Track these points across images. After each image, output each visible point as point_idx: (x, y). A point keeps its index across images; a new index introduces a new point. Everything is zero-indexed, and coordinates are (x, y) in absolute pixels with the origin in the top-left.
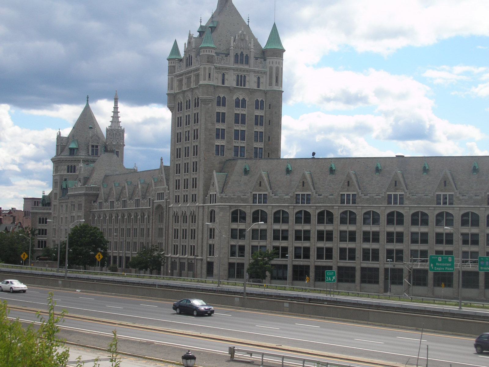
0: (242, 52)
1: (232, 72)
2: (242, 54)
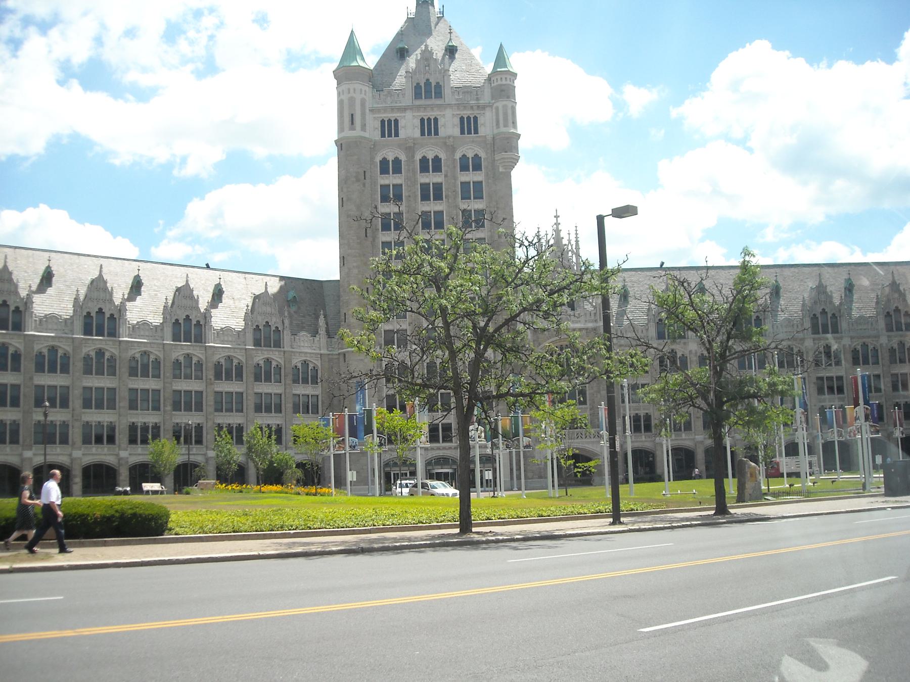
0: (428, 80)
1: (409, 114)
2: (428, 83)
